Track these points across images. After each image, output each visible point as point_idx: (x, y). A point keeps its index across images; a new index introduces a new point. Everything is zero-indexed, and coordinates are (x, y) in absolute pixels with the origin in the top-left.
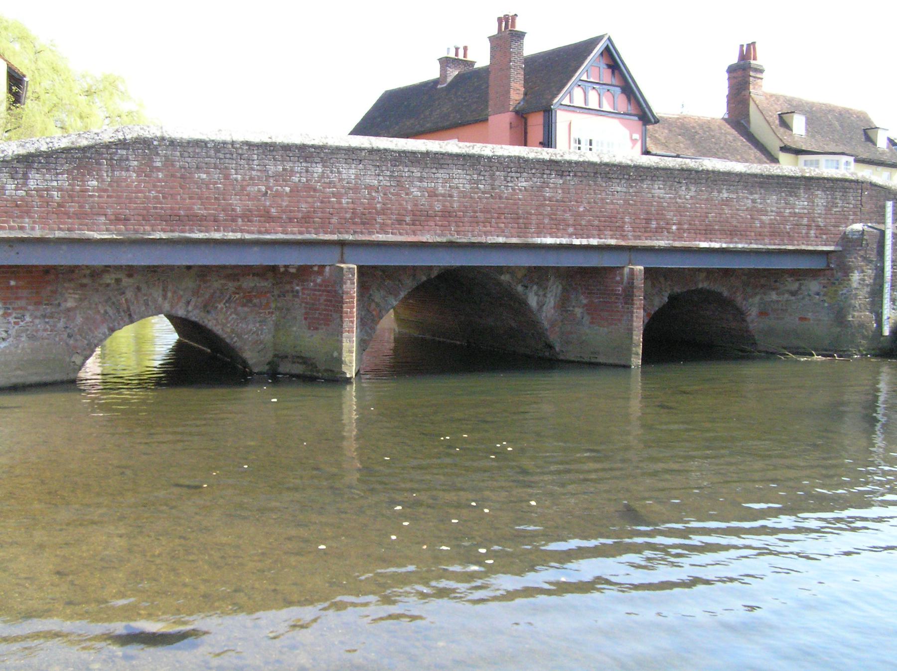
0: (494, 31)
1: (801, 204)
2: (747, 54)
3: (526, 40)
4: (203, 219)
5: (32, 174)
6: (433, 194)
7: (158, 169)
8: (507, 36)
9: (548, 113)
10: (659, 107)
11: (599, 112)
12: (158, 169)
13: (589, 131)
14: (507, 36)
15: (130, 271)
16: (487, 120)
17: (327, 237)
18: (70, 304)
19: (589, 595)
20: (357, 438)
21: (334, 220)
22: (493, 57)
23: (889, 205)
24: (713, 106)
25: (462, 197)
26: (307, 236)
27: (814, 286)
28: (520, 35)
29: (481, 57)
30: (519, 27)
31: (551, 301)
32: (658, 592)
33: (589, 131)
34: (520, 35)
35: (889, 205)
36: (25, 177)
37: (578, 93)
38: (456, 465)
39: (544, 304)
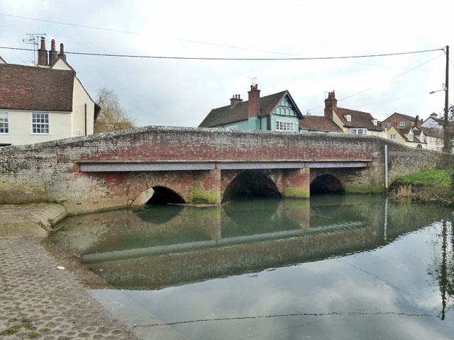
0: (250, 90)
1: (359, 146)
2: (332, 95)
3: (261, 93)
4: (173, 156)
5: (119, 142)
6: (244, 146)
7: (158, 140)
8: (254, 91)
9: (268, 117)
10: (304, 113)
11: (290, 116)
12: (158, 140)
13: (283, 122)
14: (254, 91)
15: (148, 172)
16: (247, 119)
17: (211, 161)
18: (128, 183)
19: (226, 279)
20: (337, 224)
21: (214, 155)
22: (249, 97)
23: (386, 146)
24: (320, 112)
25: (245, 148)
26: (204, 161)
27: (363, 172)
28: (259, 91)
29: (245, 98)
30: (258, 89)
31: (280, 179)
32: (279, 269)
33: (283, 122)
34: (259, 91)
35: (386, 146)
36: (116, 143)
37: (278, 110)
38: (325, 232)
39: (278, 181)
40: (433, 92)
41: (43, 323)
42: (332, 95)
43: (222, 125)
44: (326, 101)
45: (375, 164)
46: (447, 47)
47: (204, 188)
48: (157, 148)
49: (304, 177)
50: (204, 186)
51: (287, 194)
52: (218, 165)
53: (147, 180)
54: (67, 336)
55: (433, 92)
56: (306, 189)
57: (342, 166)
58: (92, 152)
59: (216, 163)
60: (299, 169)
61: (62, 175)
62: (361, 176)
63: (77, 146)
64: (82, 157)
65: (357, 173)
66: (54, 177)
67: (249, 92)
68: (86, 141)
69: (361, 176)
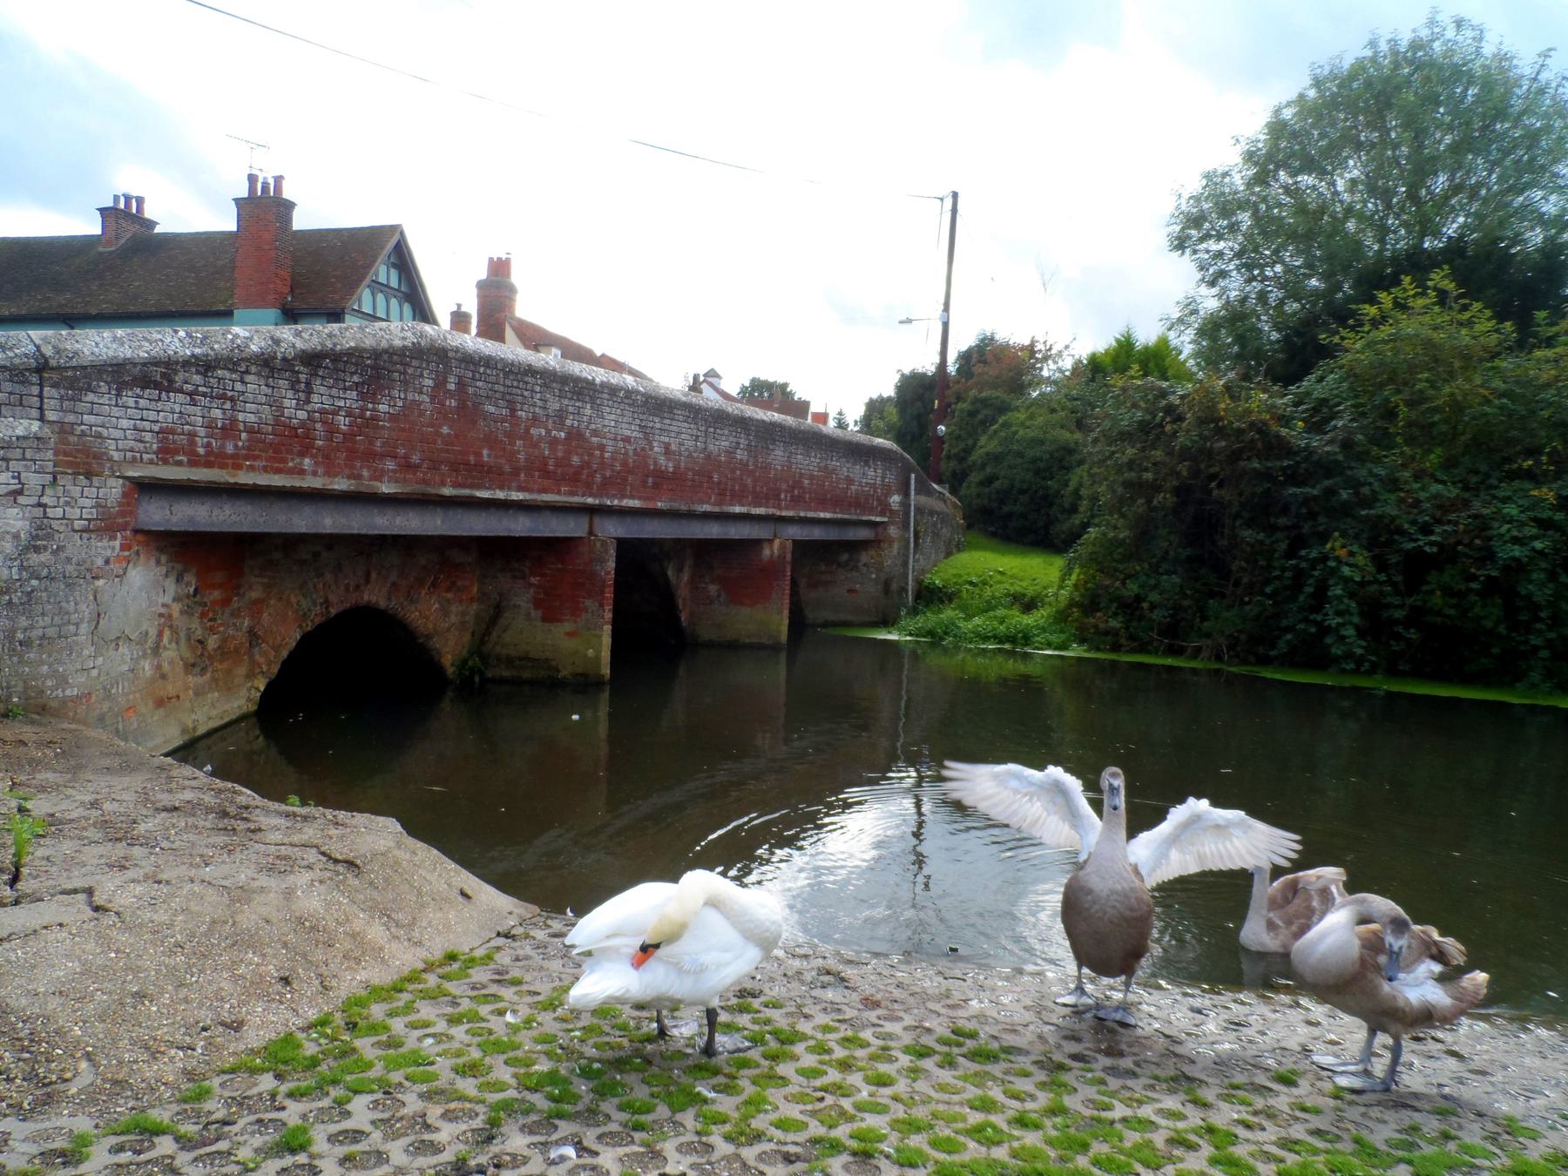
2: (499, 269)
30: (287, 194)
31: (686, 576)
36: (309, 391)
40: (909, 321)
41: (1160, 1112)
42: (499, 269)
43: (71, 320)
44: (482, 286)
45: (893, 531)
46: (955, 195)
47: (536, 614)
48: (445, 430)
49: (770, 571)
50: (537, 604)
51: (706, 633)
52: (597, 520)
53: (328, 576)
54: (1265, 1123)
55: (909, 321)
56: (780, 612)
57: (330, 522)
58: (210, 425)
59: (591, 511)
60: (757, 543)
61: (76, 547)
62: (855, 568)
63: (145, 382)
64: (166, 453)
65: (845, 557)
66: (34, 559)
67: (237, 201)
68: (187, 363)
69: (855, 568)
